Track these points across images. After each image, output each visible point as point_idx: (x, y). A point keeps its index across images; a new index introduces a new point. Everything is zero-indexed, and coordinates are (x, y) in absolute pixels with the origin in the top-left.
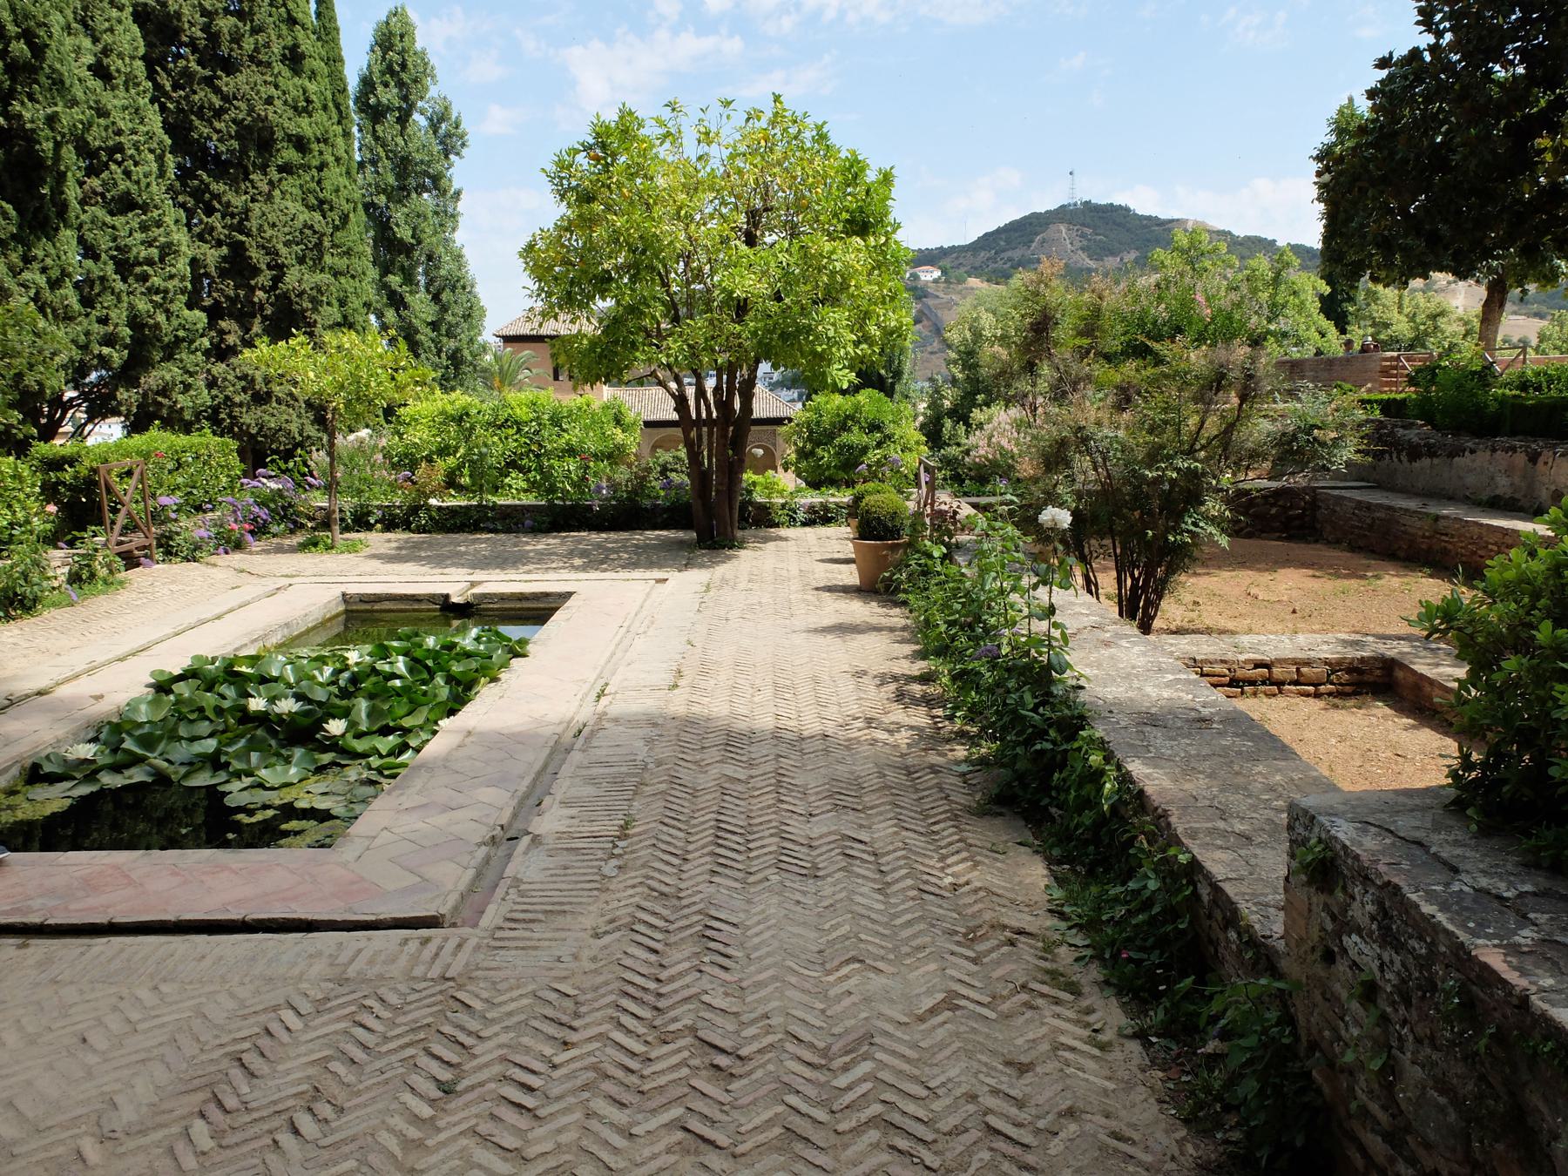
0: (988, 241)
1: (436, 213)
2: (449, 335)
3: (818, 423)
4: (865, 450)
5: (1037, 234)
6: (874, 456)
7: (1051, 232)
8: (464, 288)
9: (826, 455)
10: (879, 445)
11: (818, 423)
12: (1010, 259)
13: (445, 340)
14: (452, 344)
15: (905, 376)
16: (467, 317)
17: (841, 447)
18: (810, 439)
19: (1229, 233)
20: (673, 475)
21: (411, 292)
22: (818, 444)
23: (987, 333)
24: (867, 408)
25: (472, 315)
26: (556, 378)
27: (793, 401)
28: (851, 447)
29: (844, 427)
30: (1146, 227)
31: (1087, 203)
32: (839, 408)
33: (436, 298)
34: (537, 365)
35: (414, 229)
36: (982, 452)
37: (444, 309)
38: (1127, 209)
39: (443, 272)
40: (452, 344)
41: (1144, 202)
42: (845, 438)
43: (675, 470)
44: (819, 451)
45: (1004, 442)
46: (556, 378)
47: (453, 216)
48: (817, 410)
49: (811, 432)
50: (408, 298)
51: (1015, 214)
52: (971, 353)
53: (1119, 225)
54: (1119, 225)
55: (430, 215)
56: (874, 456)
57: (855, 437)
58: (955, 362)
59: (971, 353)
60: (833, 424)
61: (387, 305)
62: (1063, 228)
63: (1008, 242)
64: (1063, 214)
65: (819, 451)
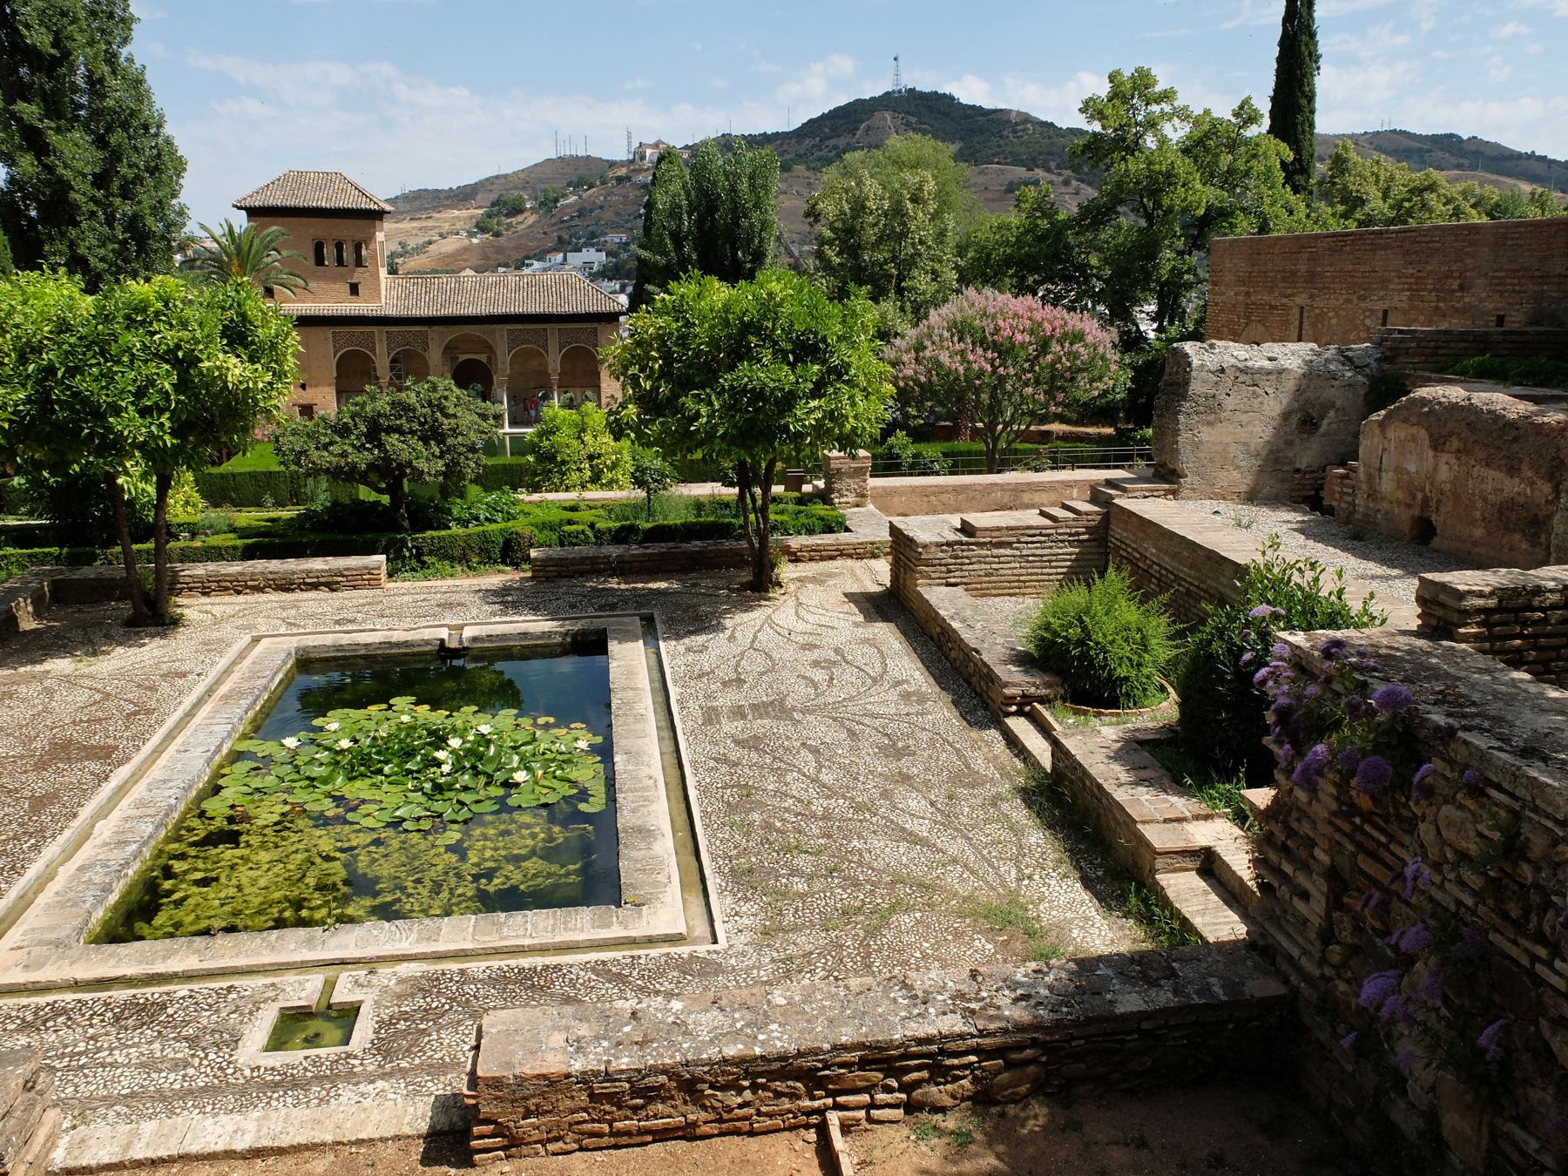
0: (812, 127)
1: (93, 13)
2: (126, 193)
3: (683, 340)
4: (788, 401)
5: (862, 122)
6: (808, 413)
7: (876, 120)
8: (146, 127)
9: (703, 409)
10: (818, 391)
11: (683, 340)
12: (835, 147)
13: (118, 201)
14: (128, 208)
15: (768, 260)
16: (154, 170)
17: (736, 392)
18: (665, 374)
19: (1052, 124)
20: (392, 440)
21: (58, 130)
22: (684, 384)
23: (871, 204)
24: (786, 310)
25: (164, 166)
26: (320, 261)
27: (614, 292)
28: (758, 395)
29: (739, 352)
30: (970, 116)
31: (912, 90)
32: (727, 308)
33: (101, 142)
34: (286, 245)
35: (57, 34)
36: (910, 372)
37: (116, 156)
38: (951, 98)
39: (110, 102)
40: (128, 208)
41: (972, 92)
42: (747, 374)
43: (398, 430)
44: (688, 402)
45: (944, 358)
46: (320, 261)
47: (123, 20)
48: (678, 311)
49: (667, 356)
50: (53, 138)
51: (842, 101)
52: (850, 231)
53: (944, 114)
54: (944, 114)
55: (82, 14)
56: (808, 413)
57: (766, 373)
58: (830, 243)
59: (850, 231)
60: (714, 342)
61: (20, 147)
62: (887, 115)
63: (833, 129)
64: (888, 101)
65: (688, 402)
